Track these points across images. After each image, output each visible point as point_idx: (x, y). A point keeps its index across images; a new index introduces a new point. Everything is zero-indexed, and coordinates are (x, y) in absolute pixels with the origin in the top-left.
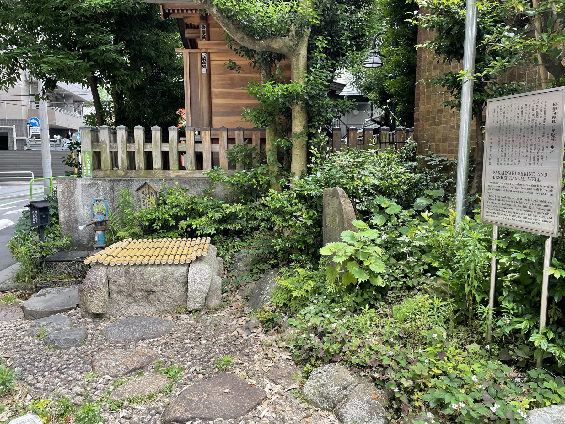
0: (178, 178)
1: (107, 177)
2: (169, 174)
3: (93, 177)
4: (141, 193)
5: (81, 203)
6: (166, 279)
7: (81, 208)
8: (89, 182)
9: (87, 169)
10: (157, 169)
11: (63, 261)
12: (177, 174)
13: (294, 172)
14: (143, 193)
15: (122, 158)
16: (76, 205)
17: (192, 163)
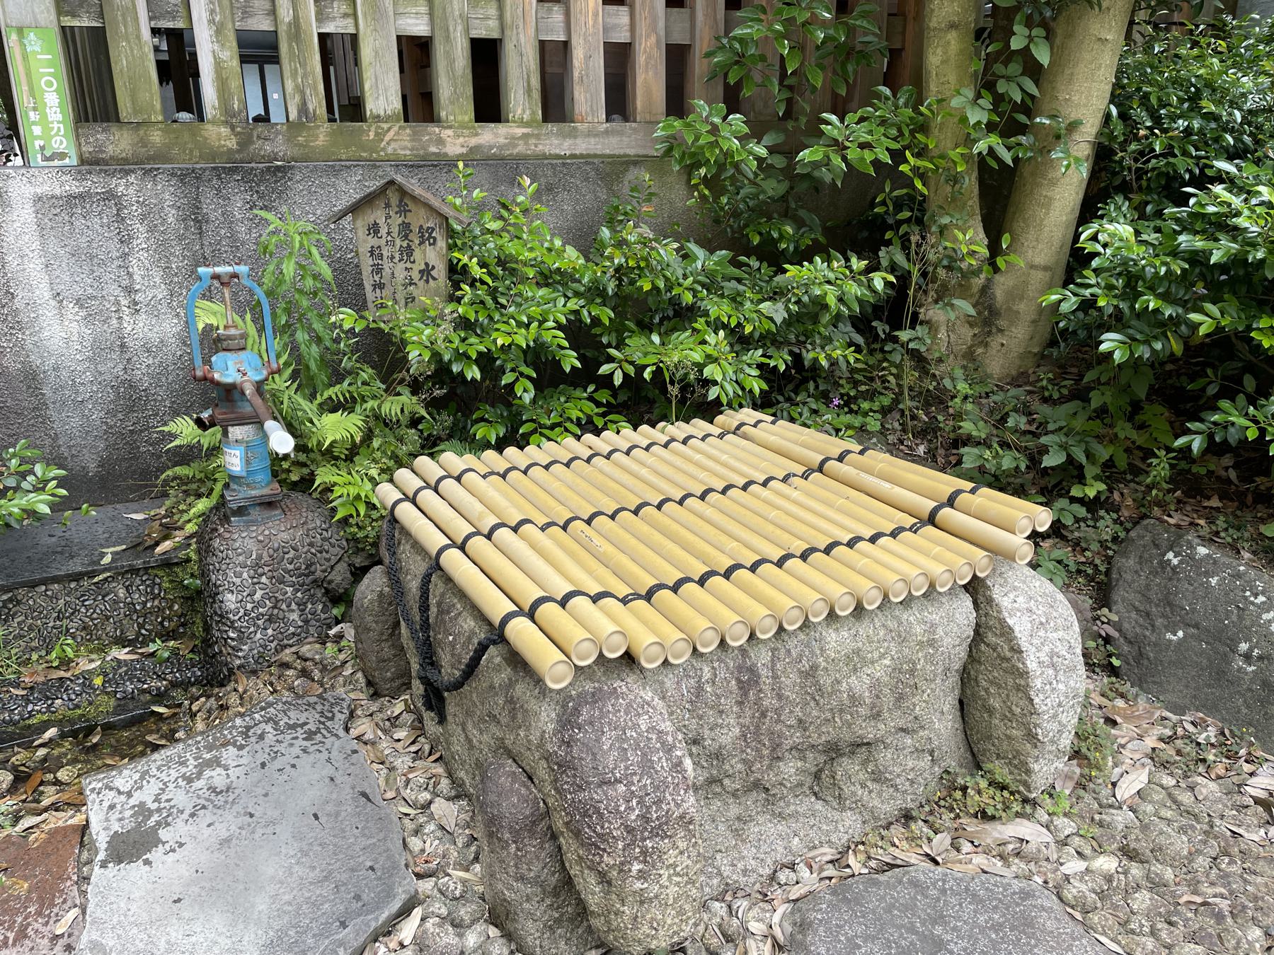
0: (474, 158)
1: (151, 159)
2: (440, 142)
3: (83, 161)
4: (362, 232)
5: (43, 292)
6: (912, 672)
7: (48, 313)
8: (73, 187)
9: (44, 121)
10: (388, 119)
11: (44, 582)
12: (473, 141)
13: (1074, 116)
14: (374, 229)
15: (218, 64)
16: (18, 303)
17: (529, 91)
